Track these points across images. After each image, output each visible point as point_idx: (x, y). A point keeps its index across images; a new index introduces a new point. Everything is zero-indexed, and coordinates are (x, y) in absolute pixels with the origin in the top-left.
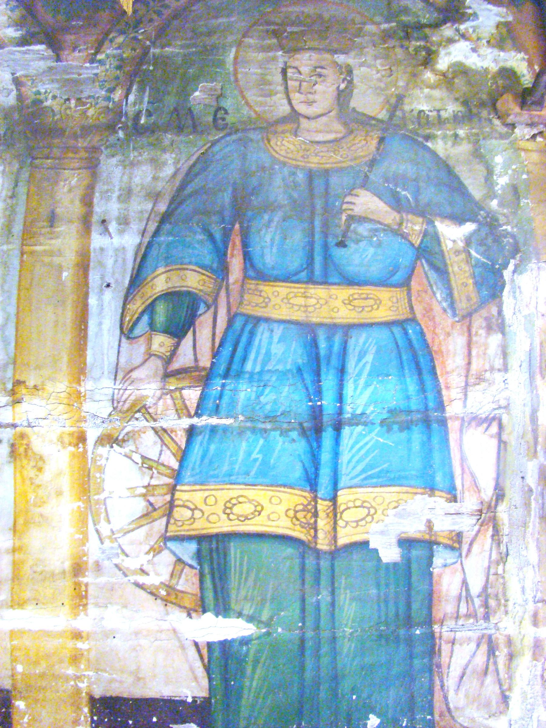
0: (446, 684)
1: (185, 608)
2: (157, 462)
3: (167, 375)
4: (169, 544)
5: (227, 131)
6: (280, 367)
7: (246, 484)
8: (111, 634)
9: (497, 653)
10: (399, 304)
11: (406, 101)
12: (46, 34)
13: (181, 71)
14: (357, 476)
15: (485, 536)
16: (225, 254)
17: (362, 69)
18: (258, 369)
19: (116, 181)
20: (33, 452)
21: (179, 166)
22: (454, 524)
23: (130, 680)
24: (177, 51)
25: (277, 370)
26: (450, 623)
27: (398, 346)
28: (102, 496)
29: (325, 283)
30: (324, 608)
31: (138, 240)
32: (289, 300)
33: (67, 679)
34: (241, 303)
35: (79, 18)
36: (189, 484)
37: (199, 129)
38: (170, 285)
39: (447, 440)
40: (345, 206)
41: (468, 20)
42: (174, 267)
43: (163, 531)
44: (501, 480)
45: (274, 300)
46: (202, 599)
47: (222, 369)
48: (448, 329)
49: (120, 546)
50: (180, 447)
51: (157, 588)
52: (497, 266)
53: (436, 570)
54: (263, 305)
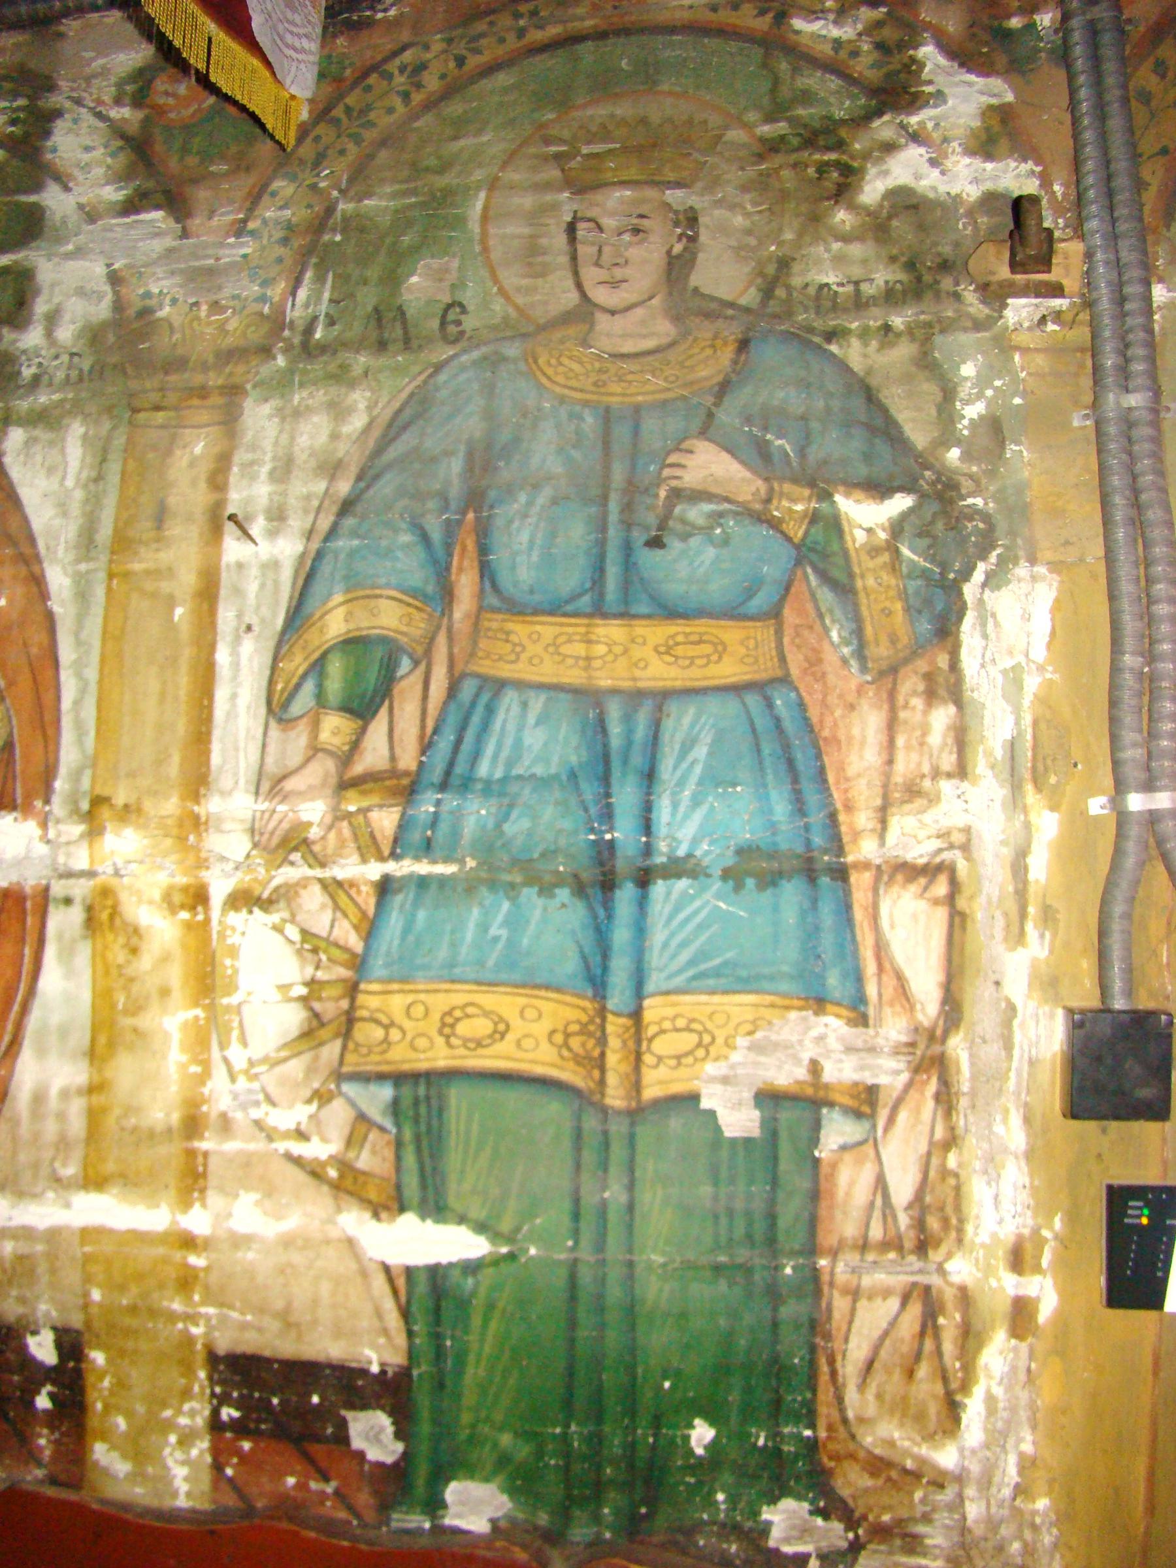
0: (840, 1372)
1: (370, 1202)
2: (327, 940)
3: (346, 785)
4: (346, 1087)
5: (464, 344)
6: (539, 770)
7: (479, 983)
8: (239, 1241)
9: (941, 1320)
10: (760, 650)
11: (796, 268)
12: (167, 193)
14: (680, 971)
15: (922, 1093)
16: (448, 568)
17: (717, 212)
18: (498, 774)
19: (268, 445)
21: (375, 413)
22: (862, 1068)
23: (274, 1325)
24: (384, 203)
25: (533, 776)
26: (849, 1258)
27: (754, 730)
28: (234, 1000)
29: (625, 615)
30: (614, 1217)
31: (300, 548)
32: (557, 646)
33: (172, 1317)
34: (473, 654)
35: (223, 157)
36: (381, 981)
37: (415, 344)
38: (352, 626)
39: (848, 907)
40: (666, 472)
41: (926, 104)
42: (361, 593)
43: (336, 1064)
44: (953, 987)
45: (533, 649)
46: (398, 1187)
47: (436, 775)
48: (851, 698)
49: (264, 1090)
50: (364, 913)
51: (323, 1165)
52: (952, 576)
53: (823, 1152)
54: (513, 657)
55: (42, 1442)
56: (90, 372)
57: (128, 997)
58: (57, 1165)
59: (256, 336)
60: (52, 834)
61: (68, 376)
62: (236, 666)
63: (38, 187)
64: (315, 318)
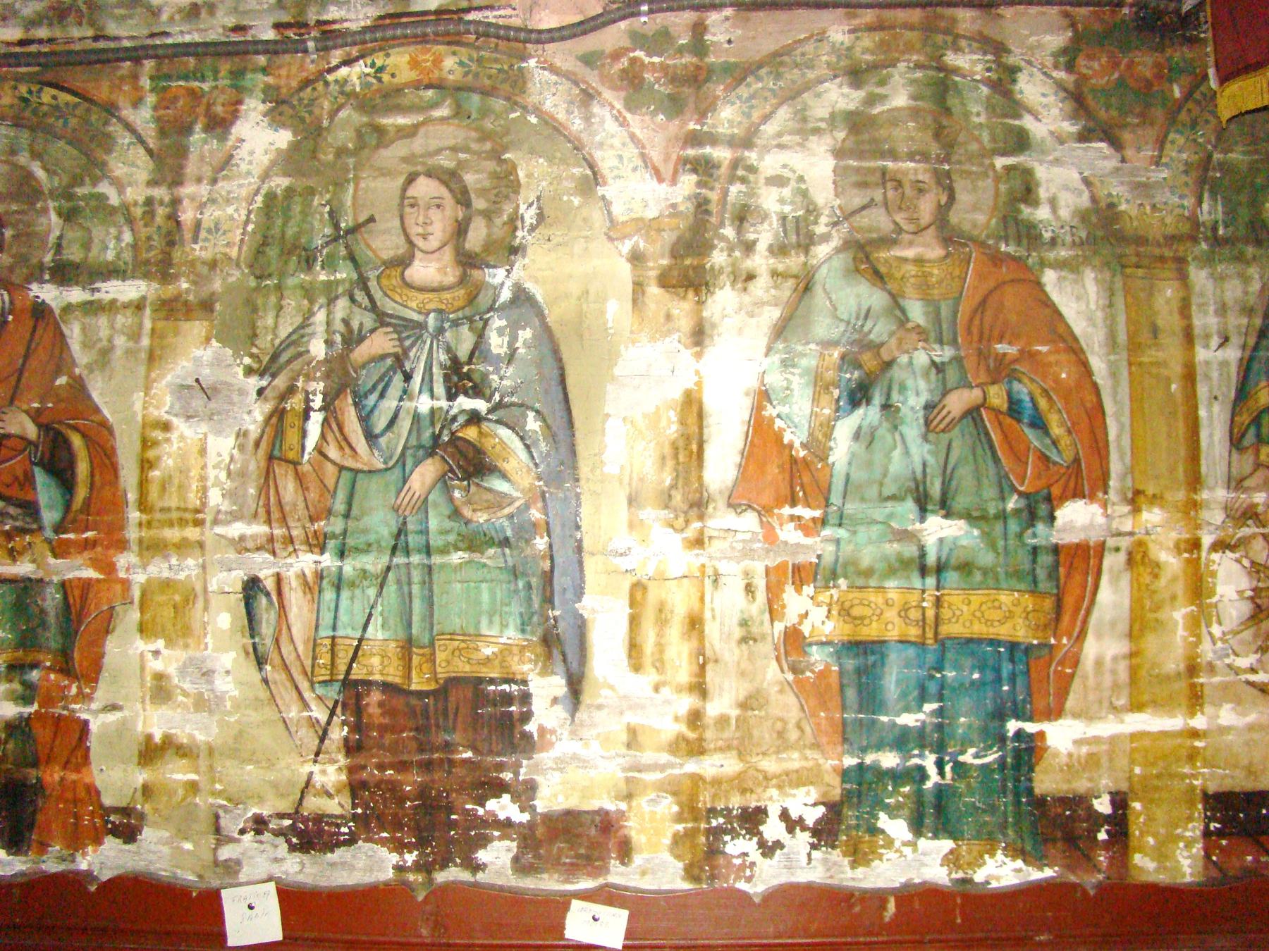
8: (1223, 730)
13: (1249, 180)
28: (1214, 600)
33: (1183, 777)
55: (1102, 858)
58: (1113, 699)
59: (1185, 228)
60: (1109, 511)
62: (1210, 417)
63: (1018, 116)
64: (1217, 222)
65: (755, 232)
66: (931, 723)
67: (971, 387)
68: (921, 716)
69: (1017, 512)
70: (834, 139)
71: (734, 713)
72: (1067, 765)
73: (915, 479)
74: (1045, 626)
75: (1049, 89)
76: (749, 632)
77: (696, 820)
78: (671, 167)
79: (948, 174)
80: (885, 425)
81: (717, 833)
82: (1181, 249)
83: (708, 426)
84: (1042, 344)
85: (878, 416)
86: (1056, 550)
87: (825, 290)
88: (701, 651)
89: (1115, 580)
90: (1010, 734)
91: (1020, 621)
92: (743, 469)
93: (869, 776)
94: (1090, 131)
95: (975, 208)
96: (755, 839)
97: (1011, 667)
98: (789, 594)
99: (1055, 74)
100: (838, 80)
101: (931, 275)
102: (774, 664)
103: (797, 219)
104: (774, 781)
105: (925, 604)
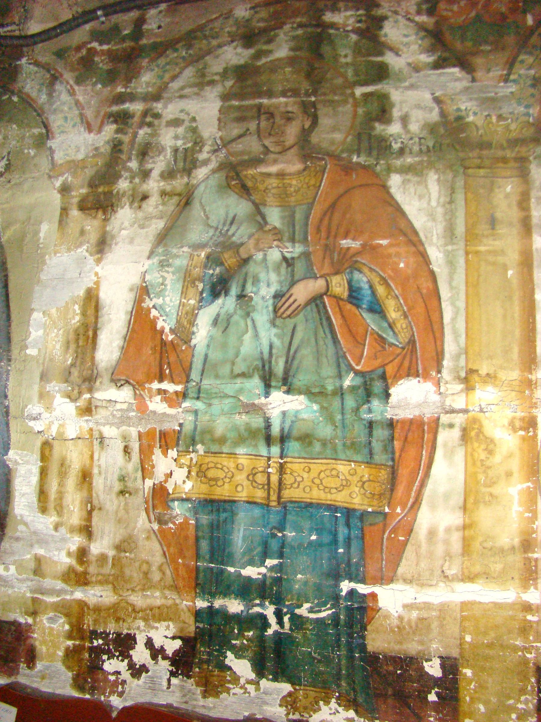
20: (484, 436)
33: (515, 649)
35: (486, 42)
56: (434, 147)
57: (486, 477)
61: (421, 149)
65: (154, 162)
66: (271, 577)
67: (316, 278)
68: (263, 570)
69: (353, 389)
70: (224, 87)
71: (111, 553)
72: (398, 627)
73: (262, 359)
74: (380, 495)
75: (411, 30)
76: (126, 487)
77: (82, 638)
78: (99, 121)
79: (314, 105)
80: (239, 312)
81: (97, 652)
82: (523, 151)
83: (103, 316)
84: (384, 238)
85: (233, 305)
86: (391, 424)
87: (201, 203)
88: (89, 500)
89: (450, 453)
90: (344, 593)
91: (357, 489)
92: (125, 350)
93: (218, 620)
94: (445, 60)
95: (334, 129)
96: (126, 661)
97: (346, 531)
98: (157, 455)
99: (417, 19)
100: (235, 44)
101: (291, 186)
102: (144, 514)
103: (186, 150)
104: (140, 614)
105: (270, 470)
